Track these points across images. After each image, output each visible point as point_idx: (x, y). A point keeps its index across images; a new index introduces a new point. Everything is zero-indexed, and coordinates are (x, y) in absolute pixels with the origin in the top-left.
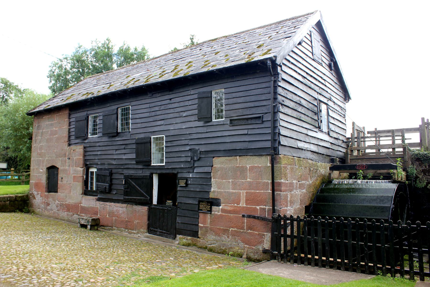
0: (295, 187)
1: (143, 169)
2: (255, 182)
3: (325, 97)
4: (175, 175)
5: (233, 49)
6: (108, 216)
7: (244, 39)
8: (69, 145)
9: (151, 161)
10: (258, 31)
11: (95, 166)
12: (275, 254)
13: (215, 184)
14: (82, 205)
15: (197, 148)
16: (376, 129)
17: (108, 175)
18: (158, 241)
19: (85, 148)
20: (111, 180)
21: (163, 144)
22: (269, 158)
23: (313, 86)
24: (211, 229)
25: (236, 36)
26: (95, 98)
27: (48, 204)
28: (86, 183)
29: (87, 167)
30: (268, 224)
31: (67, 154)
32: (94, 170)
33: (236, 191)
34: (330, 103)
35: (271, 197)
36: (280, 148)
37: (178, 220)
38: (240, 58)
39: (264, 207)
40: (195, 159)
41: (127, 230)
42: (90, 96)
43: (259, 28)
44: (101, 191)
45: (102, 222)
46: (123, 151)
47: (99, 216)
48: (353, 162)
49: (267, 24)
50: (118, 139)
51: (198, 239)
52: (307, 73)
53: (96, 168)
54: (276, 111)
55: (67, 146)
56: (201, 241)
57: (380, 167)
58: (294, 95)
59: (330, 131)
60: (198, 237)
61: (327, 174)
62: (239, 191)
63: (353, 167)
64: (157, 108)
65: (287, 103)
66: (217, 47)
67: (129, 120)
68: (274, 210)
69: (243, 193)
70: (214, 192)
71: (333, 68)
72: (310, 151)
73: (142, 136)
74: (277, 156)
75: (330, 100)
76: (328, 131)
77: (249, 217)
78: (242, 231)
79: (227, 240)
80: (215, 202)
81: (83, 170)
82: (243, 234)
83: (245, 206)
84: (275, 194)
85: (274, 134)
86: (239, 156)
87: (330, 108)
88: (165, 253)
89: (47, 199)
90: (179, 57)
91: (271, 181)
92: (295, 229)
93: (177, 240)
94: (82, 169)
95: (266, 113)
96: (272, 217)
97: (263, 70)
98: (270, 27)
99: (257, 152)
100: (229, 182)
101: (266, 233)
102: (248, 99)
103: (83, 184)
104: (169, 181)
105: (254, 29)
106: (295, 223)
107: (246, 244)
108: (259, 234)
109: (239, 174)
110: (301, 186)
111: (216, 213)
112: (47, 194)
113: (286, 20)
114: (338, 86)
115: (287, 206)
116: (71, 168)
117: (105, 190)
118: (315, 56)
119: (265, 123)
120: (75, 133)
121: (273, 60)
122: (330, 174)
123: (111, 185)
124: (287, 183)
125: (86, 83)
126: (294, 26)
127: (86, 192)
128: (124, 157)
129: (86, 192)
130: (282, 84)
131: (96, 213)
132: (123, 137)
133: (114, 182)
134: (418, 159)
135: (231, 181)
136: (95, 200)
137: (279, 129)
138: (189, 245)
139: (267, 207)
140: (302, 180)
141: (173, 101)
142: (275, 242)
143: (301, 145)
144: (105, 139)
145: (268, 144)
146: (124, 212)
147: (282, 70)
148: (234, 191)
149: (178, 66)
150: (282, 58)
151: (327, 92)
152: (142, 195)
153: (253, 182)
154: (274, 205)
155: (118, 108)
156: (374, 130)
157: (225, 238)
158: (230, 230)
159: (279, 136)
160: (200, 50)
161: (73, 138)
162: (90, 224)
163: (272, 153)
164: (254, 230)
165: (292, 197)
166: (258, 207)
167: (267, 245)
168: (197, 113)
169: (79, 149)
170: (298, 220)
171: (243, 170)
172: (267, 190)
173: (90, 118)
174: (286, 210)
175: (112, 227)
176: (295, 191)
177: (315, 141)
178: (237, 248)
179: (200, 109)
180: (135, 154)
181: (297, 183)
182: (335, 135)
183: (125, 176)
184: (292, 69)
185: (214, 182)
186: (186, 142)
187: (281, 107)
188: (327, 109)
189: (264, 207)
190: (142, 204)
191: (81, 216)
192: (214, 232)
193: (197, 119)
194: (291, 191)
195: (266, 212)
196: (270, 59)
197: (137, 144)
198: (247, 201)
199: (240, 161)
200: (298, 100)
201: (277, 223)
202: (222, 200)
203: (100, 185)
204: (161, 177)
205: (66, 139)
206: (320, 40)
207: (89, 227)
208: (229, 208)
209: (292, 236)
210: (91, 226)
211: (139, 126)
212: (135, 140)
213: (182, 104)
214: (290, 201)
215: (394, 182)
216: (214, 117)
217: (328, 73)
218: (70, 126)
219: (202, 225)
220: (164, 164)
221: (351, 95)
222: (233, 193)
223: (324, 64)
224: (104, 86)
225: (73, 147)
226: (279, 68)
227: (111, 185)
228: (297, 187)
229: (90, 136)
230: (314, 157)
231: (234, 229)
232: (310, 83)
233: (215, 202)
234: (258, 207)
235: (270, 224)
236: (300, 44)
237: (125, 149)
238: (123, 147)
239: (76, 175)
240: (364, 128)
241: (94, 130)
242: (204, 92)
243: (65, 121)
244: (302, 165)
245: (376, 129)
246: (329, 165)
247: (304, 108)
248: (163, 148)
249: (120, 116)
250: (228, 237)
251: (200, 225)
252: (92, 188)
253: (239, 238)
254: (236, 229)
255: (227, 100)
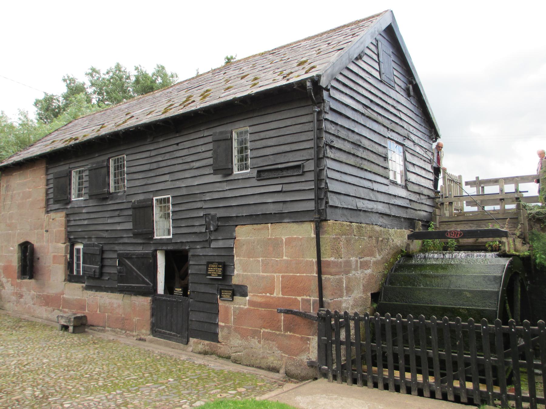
0: (353, 267)
1: (143, 243)
2: (294, 262)
3: (399, 134)
4: (187, 251)
5: (265, 71)
6: (98, 312)
7: (283, 56)
8: (47, 212)
9: (154, 233)
10: (303, 43)
11: (79, 241)
12: (319, 371)
13: (239, 265)
14: (64, 296)
15: (213, 212)
16: (477, 178)
17: (98, 253)
18: (161, 348)
19: (67, 215)
20: (102, 259)
21: (169, 209)
22: (313, 225)
23: (380, 119)
24: (236, 330)
25: (272, 53)
26: (76, 145)
27: (21, 296)
28: (70, 265)
29: (72, 243)
30: (312, 324)
31: (45, 224)
32: (81, 247)
33: (268, 274)
34: (407, 143)
35: (317, 283)
36: (329, 210)
37: (193, 316)
38: (270, 81)
39: (308, 298)
40: (212, 228)
41: (124, 332)
42: (73, 142)
43: (305, 40)
44: (90, 277)
45: (90, 320)
46: (117, 220)
47: (87, 311)
48: (443, 226)
49: (316, 33)
50: (110, 202)
51: (219, 345)
52: (371, 101)
53: (81, 243)
54: (321, 156)
55: (44, 213)
56: (222, 348)
57: (477, 237)
58: (350, 133)
59: (408, 183)
60: (219, 342)
61: (405, 245)
62: (273, 274)
63: (442, 235)
64: (159, 158)
65: (338, 144)
66: (246, 69)
67: (124, 175)
68: (321, 304)
69: (278, 277)
70: (238, 275)
71: (412, 93)
72: (377, 213)
73: (141, 197)
74: (324, 223)
75: (408, 139)
76: (406, 184)
77: (287, 312)
78: (278, 333)
79: (258, 347)
80: (240, 291)
81: (66, 247)
82: (280, 337)
83: (281, 295)
84: (323, 278)
85: (318, 189)
86: (272, 223)
87: (408, 150)
88: (165, 369)
89: (20, 288)
90: (196, 85)
91: (316, 259)
92: (352, 332)
93: (191, 346)
94: (64, 246)
95: (308, 160)
96: (318, 314)
97: (301, 96)
98: (320, 37)
99: (297, 217)
100: (258, 261)
101: (311, 337)
102: (282, 140)
103: (65, 267)
104: (177, 260)
105: (299, 42)
106: (352, 324)
107: (284, 352)
108: (302, 338)
109: (271, 249)
110: (364, 265)
111: (242, 306)
112: (19, 281)
113: (344, 26)
114: (420, 118)
115: (341, 296)
116: (50, 244)
117: (95, 275)
118: (383, 76)
119: (307, 174)
120: (54, 196)
121: (315, 81)
122: (408, 245)
123: (102, 267)
124: (341, 262)
125: (76, 125)
126: (353, 33)
127: (71, 278)
128: (119, 227)
129: (71, 278)
130: (330, 116)
131: (83, 308)
132: (116, 199)
133: (107, 262)
134: (539, 220)
135: (260, 259)
136: (81, 289)
137: (326, 183)
138: (205, 353)
139: (312, 298)
140: (365, 256)
141: (181, 146)
142: (324, 349)
143: (361, 204)
144: (91, 203)
145: (311, 206)
146: (119, 306)
147: (330, 96)
148: (265, 274)
149: (191, 96)
150: (330, 78)
151: (403, 127)
152: (144, 282)
153: (291, 261)
154: (321, 296)
155: (109, 158)
156: (475, 179)
157: (255, 343)
158: (262, 331)
159: (326, 193)
160: (225, 73)
161: (51, 201)
162: (72, 324)
163: (315, 218)
164: (294, 332)
165: (349, 282)
166: (299, 298)
167: (313, 354)
168: (212, 162)
169: (60, 217)
170: (357, 319)
171: (276, 244)
172: (311, 272)
173: (73, 174)
174: (341, 302)
175: (105, 327)
176: (353, 272)
177: (381, 198)
178: (272, 359)
179: (215, 158)
180: (131, 223)
181: (357, 261)
182: (416, 189)
183: (119, 255)
184: (346, 94)
185: (238, 262)
186: (199, 205)
187: (328, 150)
188: (404, 152)
189: (308, 298)
190: (144, 293)
191: (65, 312)
192: (239, 334)
193: (212, 172)
194: (347, 272)
195: (310, 304)
196: (312, 79)
197: (134, 208)
198: (283, 288)
199: (272, 231)
200: (357, 140)
201: (328, 324)
202: (249, 289)
203: (88, 267)
204: (170, 256)
205: (43, 204)
206: (391, 54)
207: (71, 328)
208: (259, 300)
209: (348, 343)
210: (75, 327)
211: (137, 183)
212: (131, 204)
213: (193, 151)
214: (347, 287)
215: (504, 255)
216: (235, 168)
217: (403, 100)
218: (47, 185)
219: (223, 324)
220: (171, 237)
221: (441, 132)
222: (264, 277)
223: (397, 88)
224: (94, 128)
225: (52, 215)
226: (325, 93)
227: (102, 267)
228: (357, 266)
229: (74, 198)
230: (384, 221)
231: (266, 330)
232: (376, 115)
233: (240, 291)
234: (299, 298)
235: (316, 324)
236: (359, 58)
237: (119, 216)
238: (117, 213)
239: (56, 254)
240: (460, 177)
241: (80, 190)
242: (221, 133)
243: (41, 178)
244: (365, 234)
245: (477, 178)
246: (407, 232)
247: (366, 151)
248: (169, 214)
249: (112, 170)
250: (259, 342)
251: (221, 324)
252: (78, 272)
253: (274, 343)
254: (269, 330)
255: (252, 143)
